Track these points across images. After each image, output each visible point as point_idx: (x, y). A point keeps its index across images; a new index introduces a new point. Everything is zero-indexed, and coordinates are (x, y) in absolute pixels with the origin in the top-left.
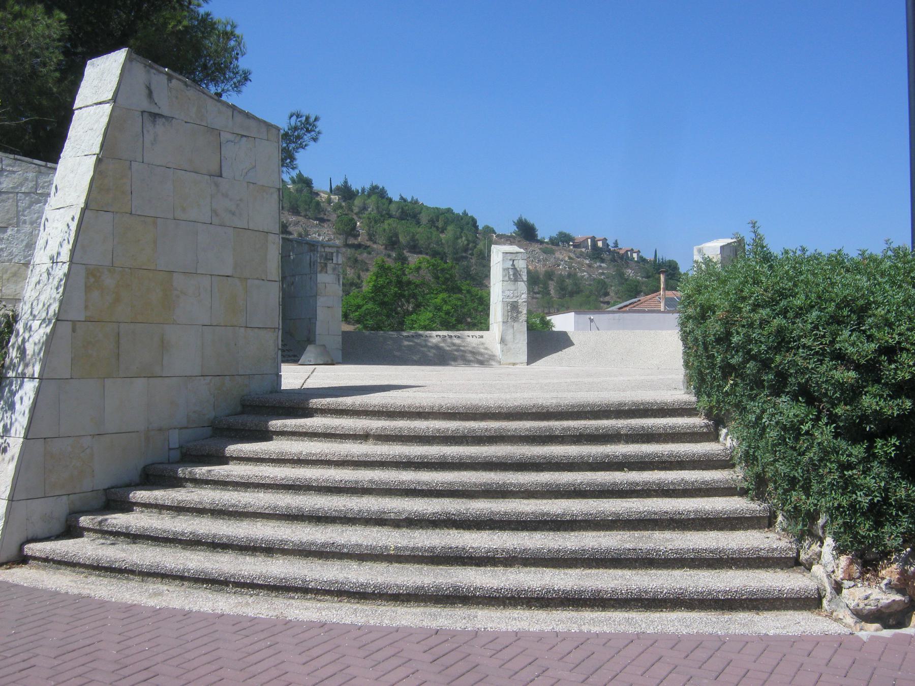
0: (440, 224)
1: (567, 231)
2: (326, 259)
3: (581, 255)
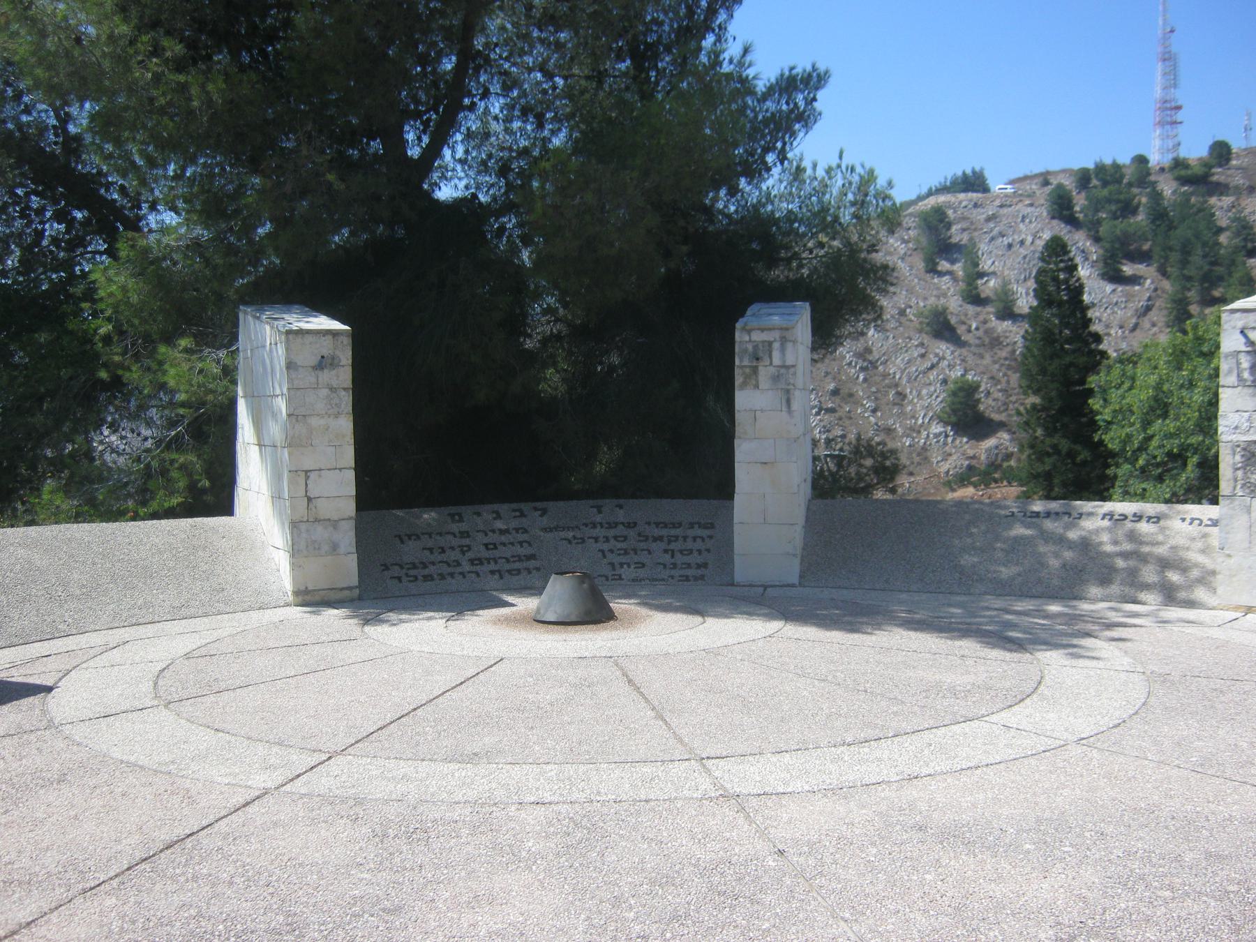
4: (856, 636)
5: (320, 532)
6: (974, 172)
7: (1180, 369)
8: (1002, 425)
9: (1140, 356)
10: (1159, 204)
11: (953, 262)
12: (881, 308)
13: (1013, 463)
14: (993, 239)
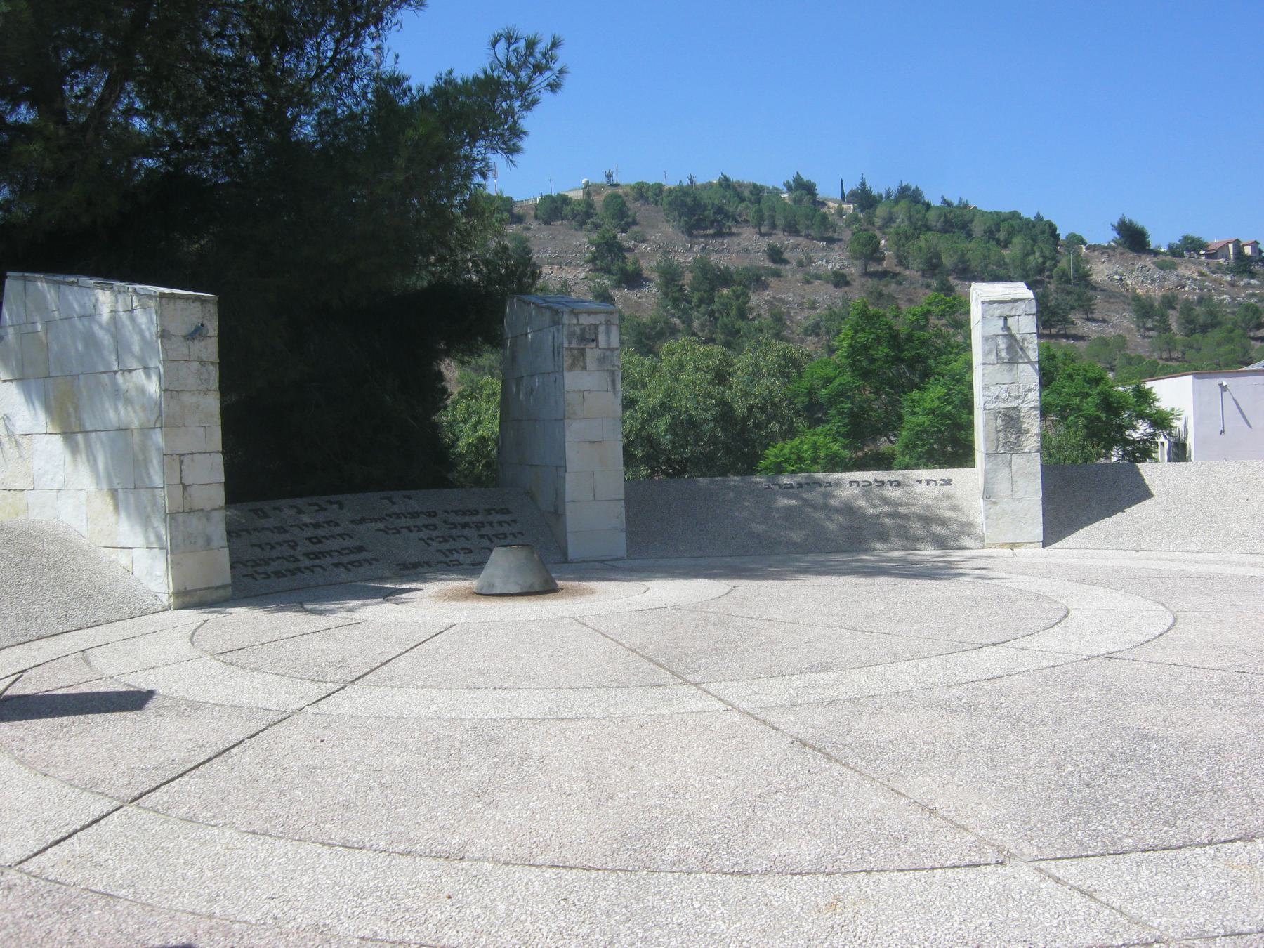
0: (1002, 236)
1: (1196, 235)
2: (583, 339)
3: (1219, 268)
5: (196, 523)
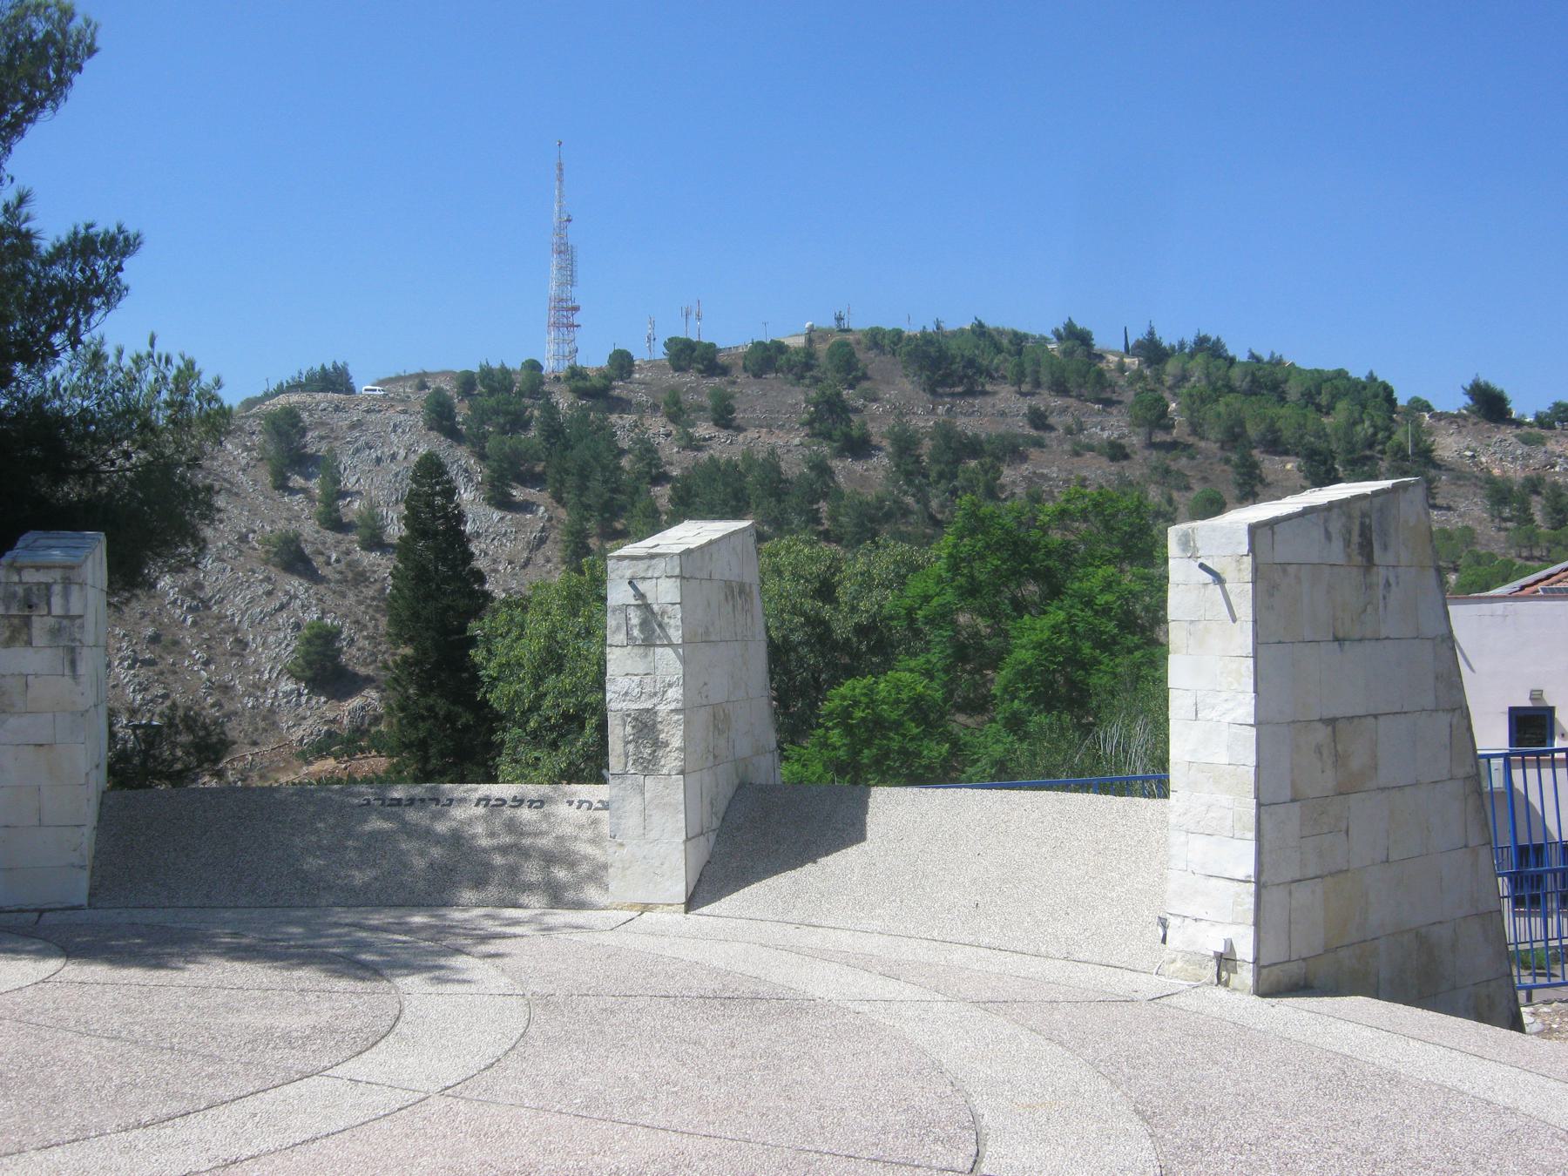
4: (163, 973)
6: (335, 367)
7: (576, 615)
8: (368, 681)
9: (529, 600)
10: (553, 419)
11: (308, 478)
12: (204, 540)
13: (382, 727)
14: (357, 451)
